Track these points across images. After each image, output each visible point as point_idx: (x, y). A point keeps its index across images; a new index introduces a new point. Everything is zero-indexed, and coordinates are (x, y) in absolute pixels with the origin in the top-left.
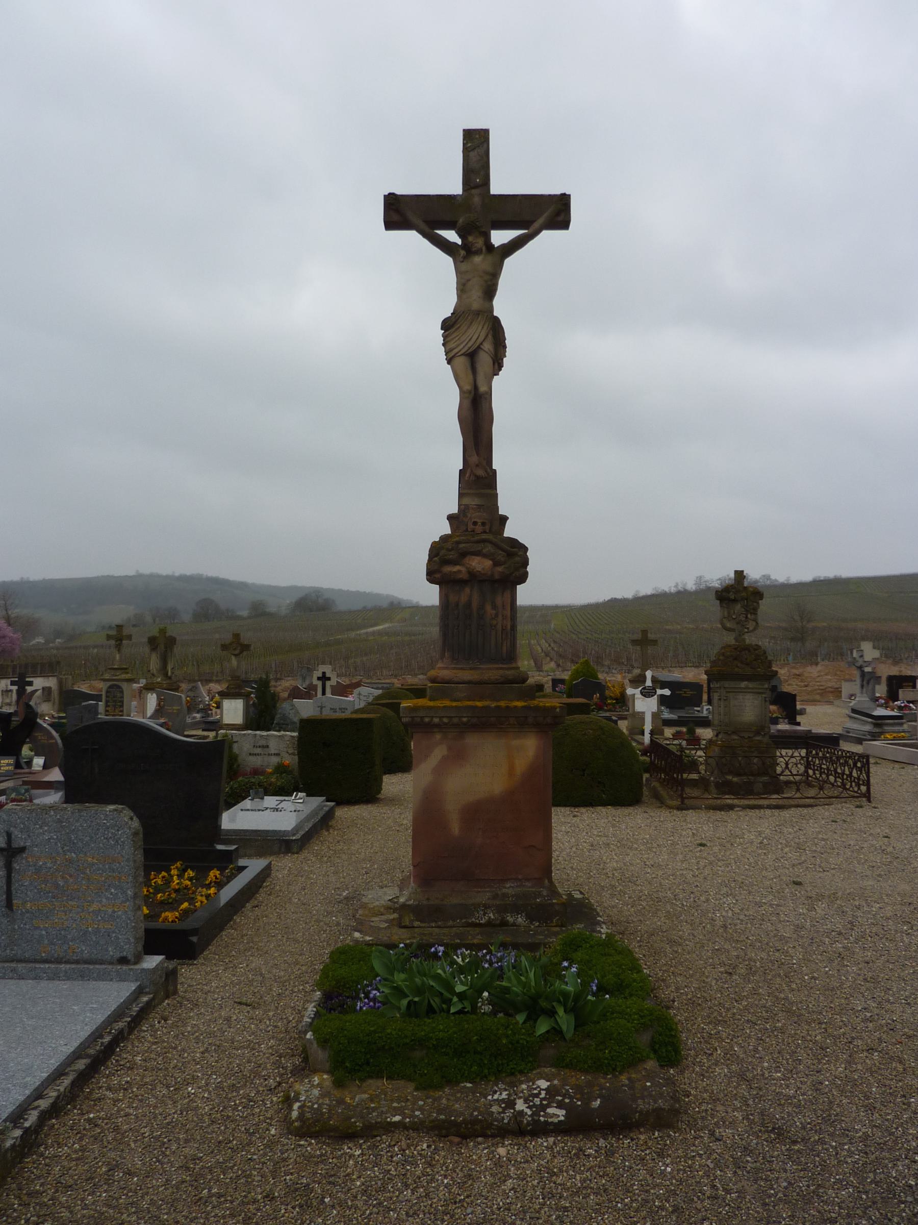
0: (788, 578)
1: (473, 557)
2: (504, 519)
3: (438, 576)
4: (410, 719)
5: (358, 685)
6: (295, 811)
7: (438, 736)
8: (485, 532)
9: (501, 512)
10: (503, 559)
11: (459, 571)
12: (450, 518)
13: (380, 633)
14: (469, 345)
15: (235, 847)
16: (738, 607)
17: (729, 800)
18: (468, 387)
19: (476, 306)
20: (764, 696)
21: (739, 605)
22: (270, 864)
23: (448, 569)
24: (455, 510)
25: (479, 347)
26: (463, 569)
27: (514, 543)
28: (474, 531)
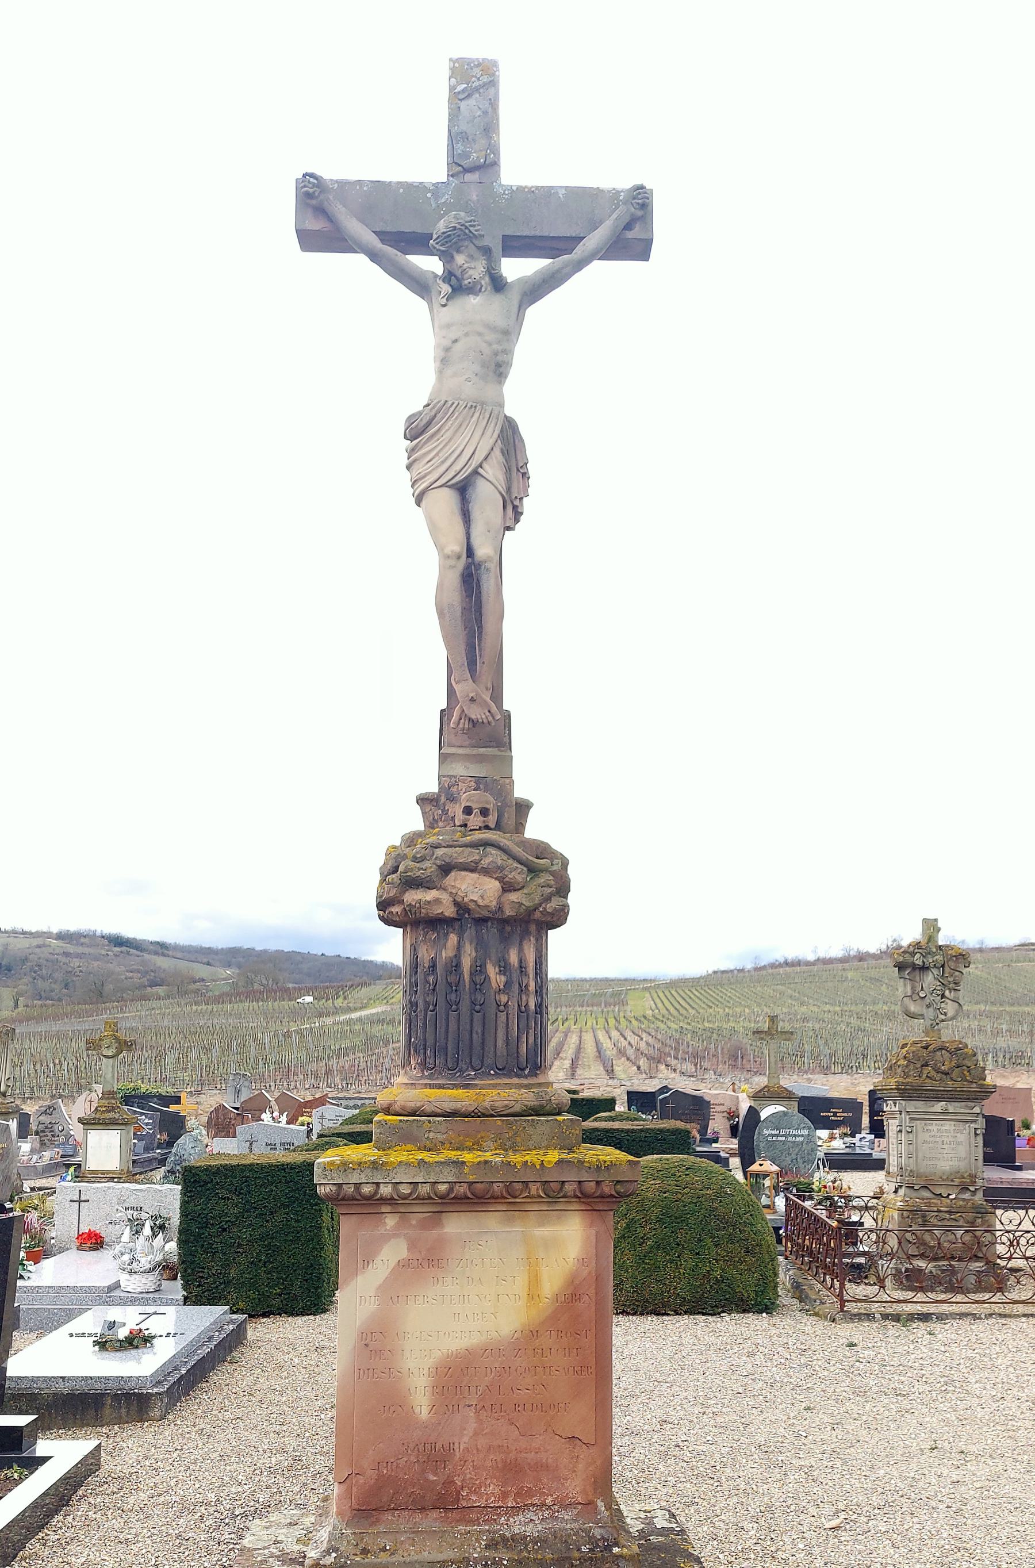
0: (963, 942)
1: (463, 873)
2: (523, 808)
3: (396, 909)
4: (334, 1188)
5: (321, 1101)
6: (168, 1335)
7: (390, 1221)
8: (487, 827)
9: (520, 791)
10: (520, 878)
11: (437, 901)
12: (423, 800)
13: (372, 1020)
14: (457, 467)
15: (30, 1418)
16: (929, 979)
17: (919, 1302)
18: (455, 545)
19: (470, 390)
20: (973, 1125)
21: (931, 976)
22: (99, 1446)
23: (413, 896)
24: (433, 787)
25: (475, 472)
26: (444, 897)
27: (542, 850)
28: (465, 825)
